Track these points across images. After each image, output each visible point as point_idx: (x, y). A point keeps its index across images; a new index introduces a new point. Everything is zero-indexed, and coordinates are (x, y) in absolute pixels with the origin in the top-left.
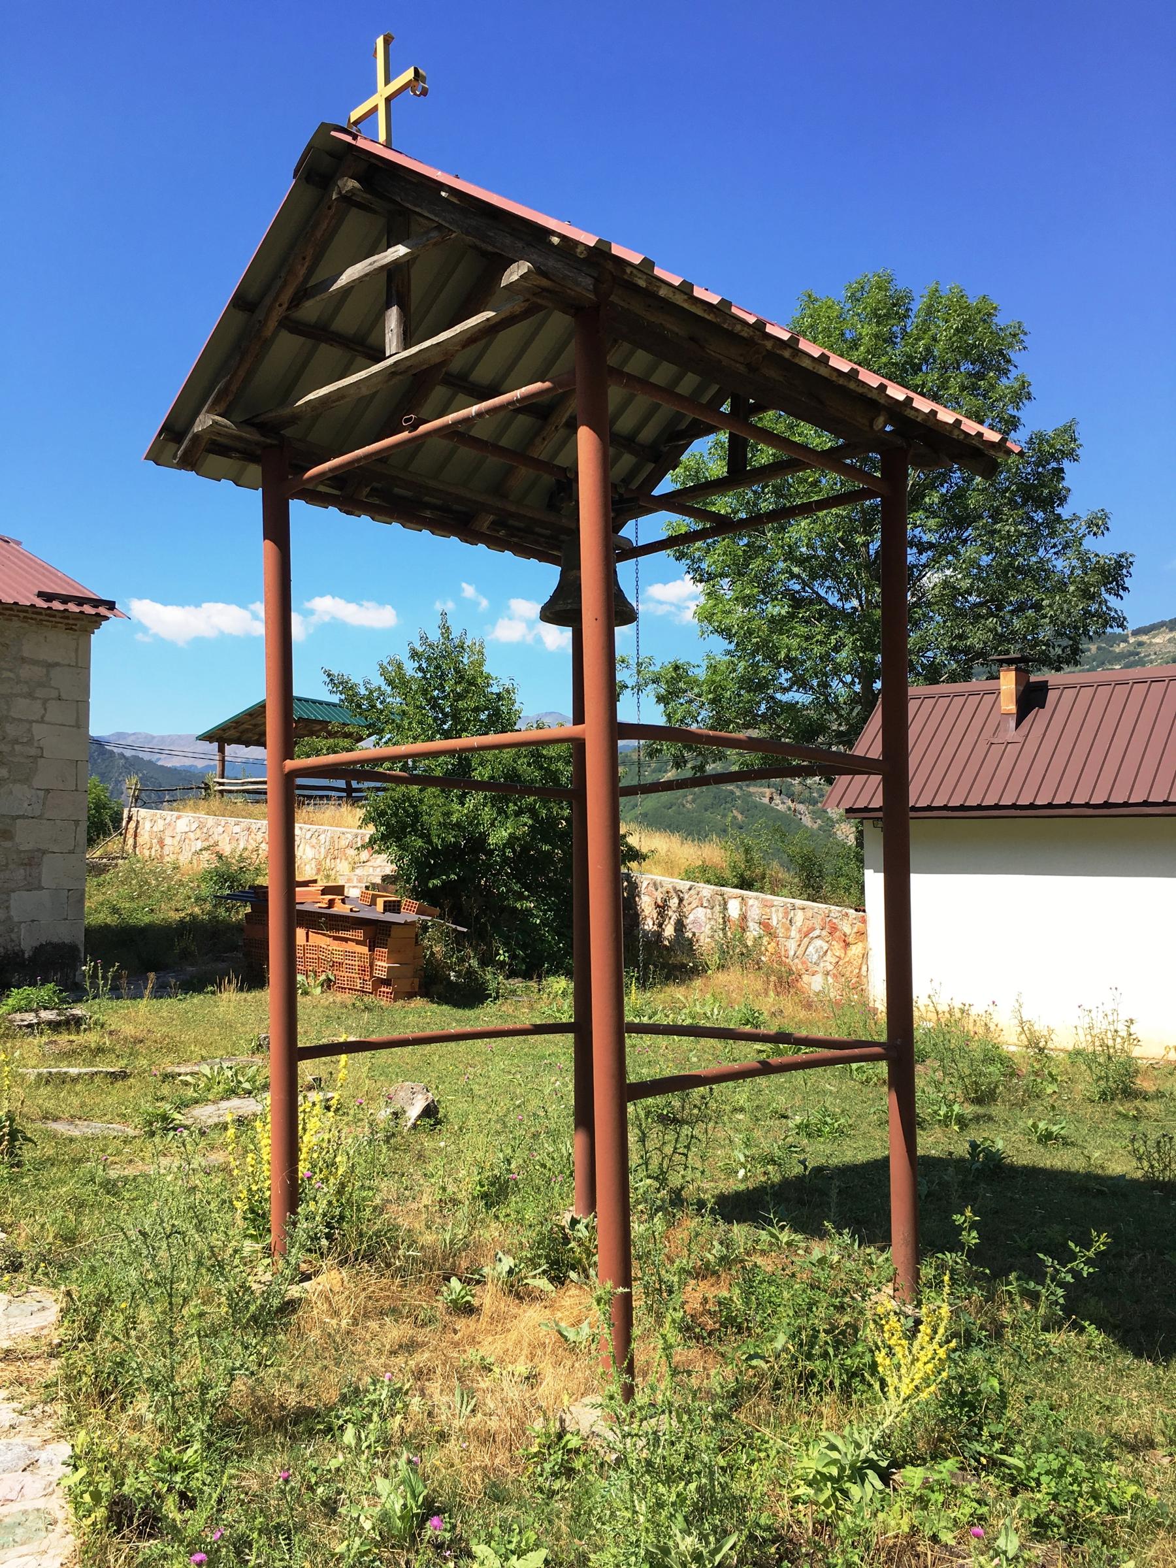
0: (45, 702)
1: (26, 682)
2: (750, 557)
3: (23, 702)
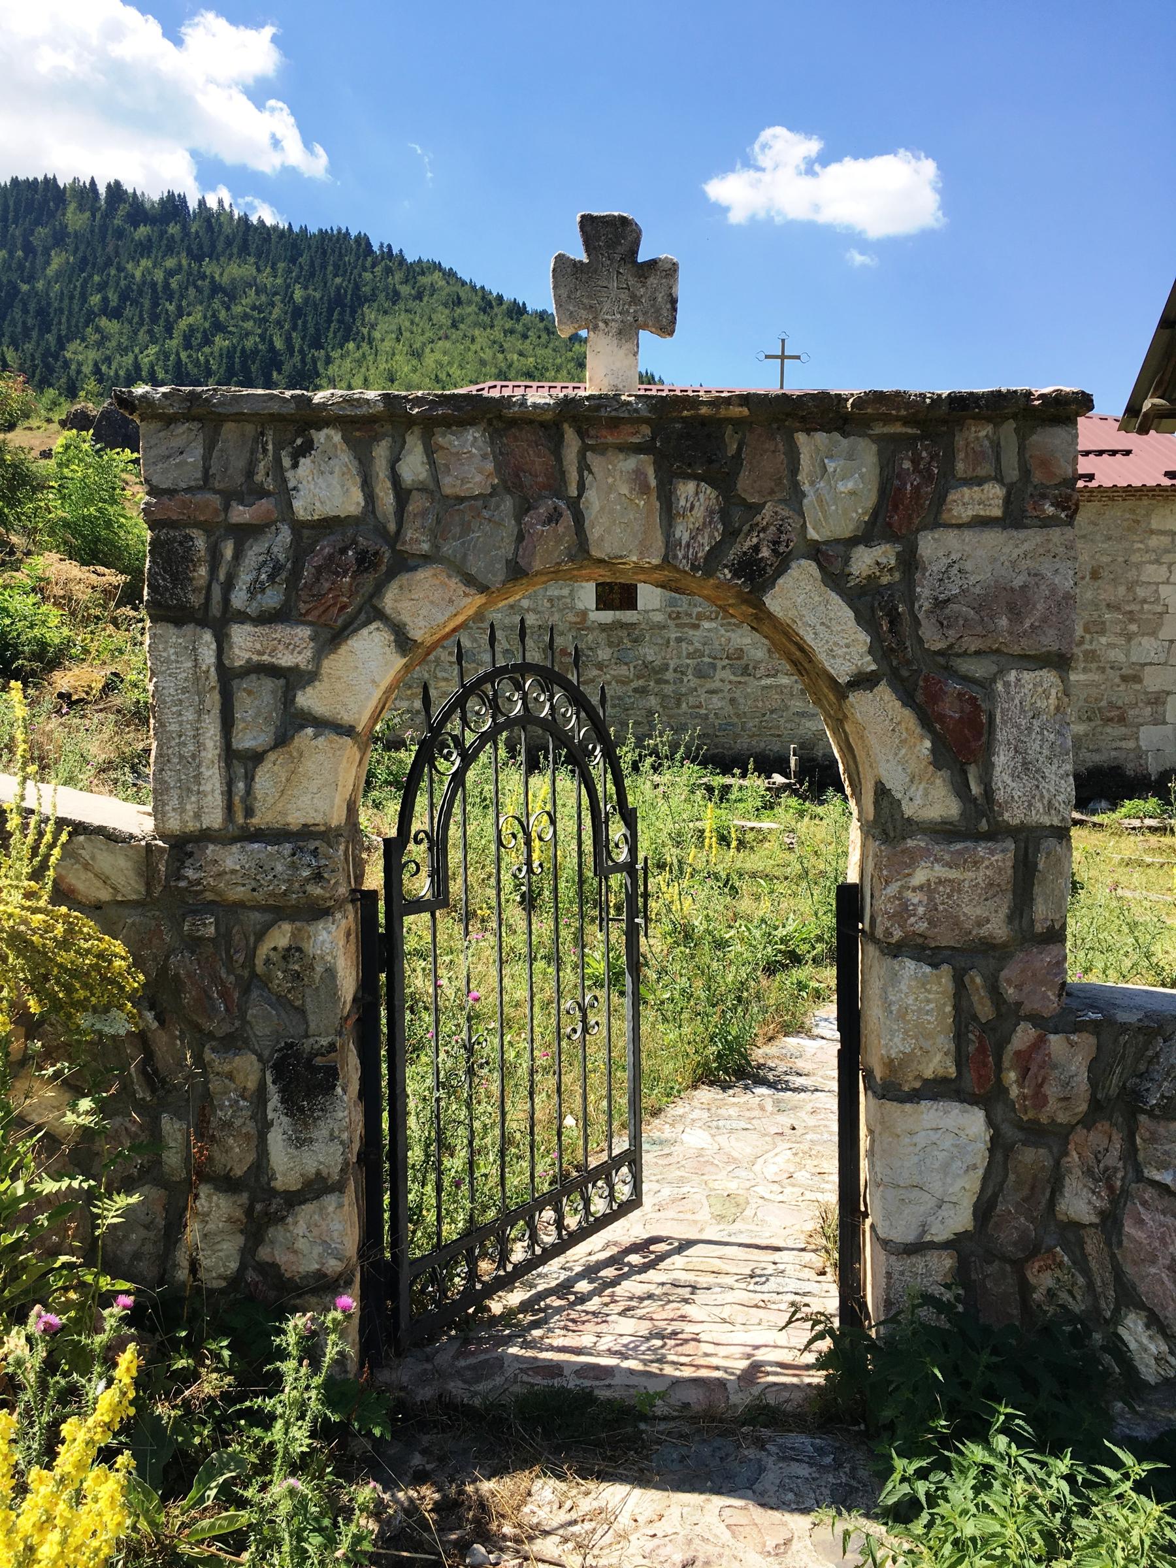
3: (1150, 568)
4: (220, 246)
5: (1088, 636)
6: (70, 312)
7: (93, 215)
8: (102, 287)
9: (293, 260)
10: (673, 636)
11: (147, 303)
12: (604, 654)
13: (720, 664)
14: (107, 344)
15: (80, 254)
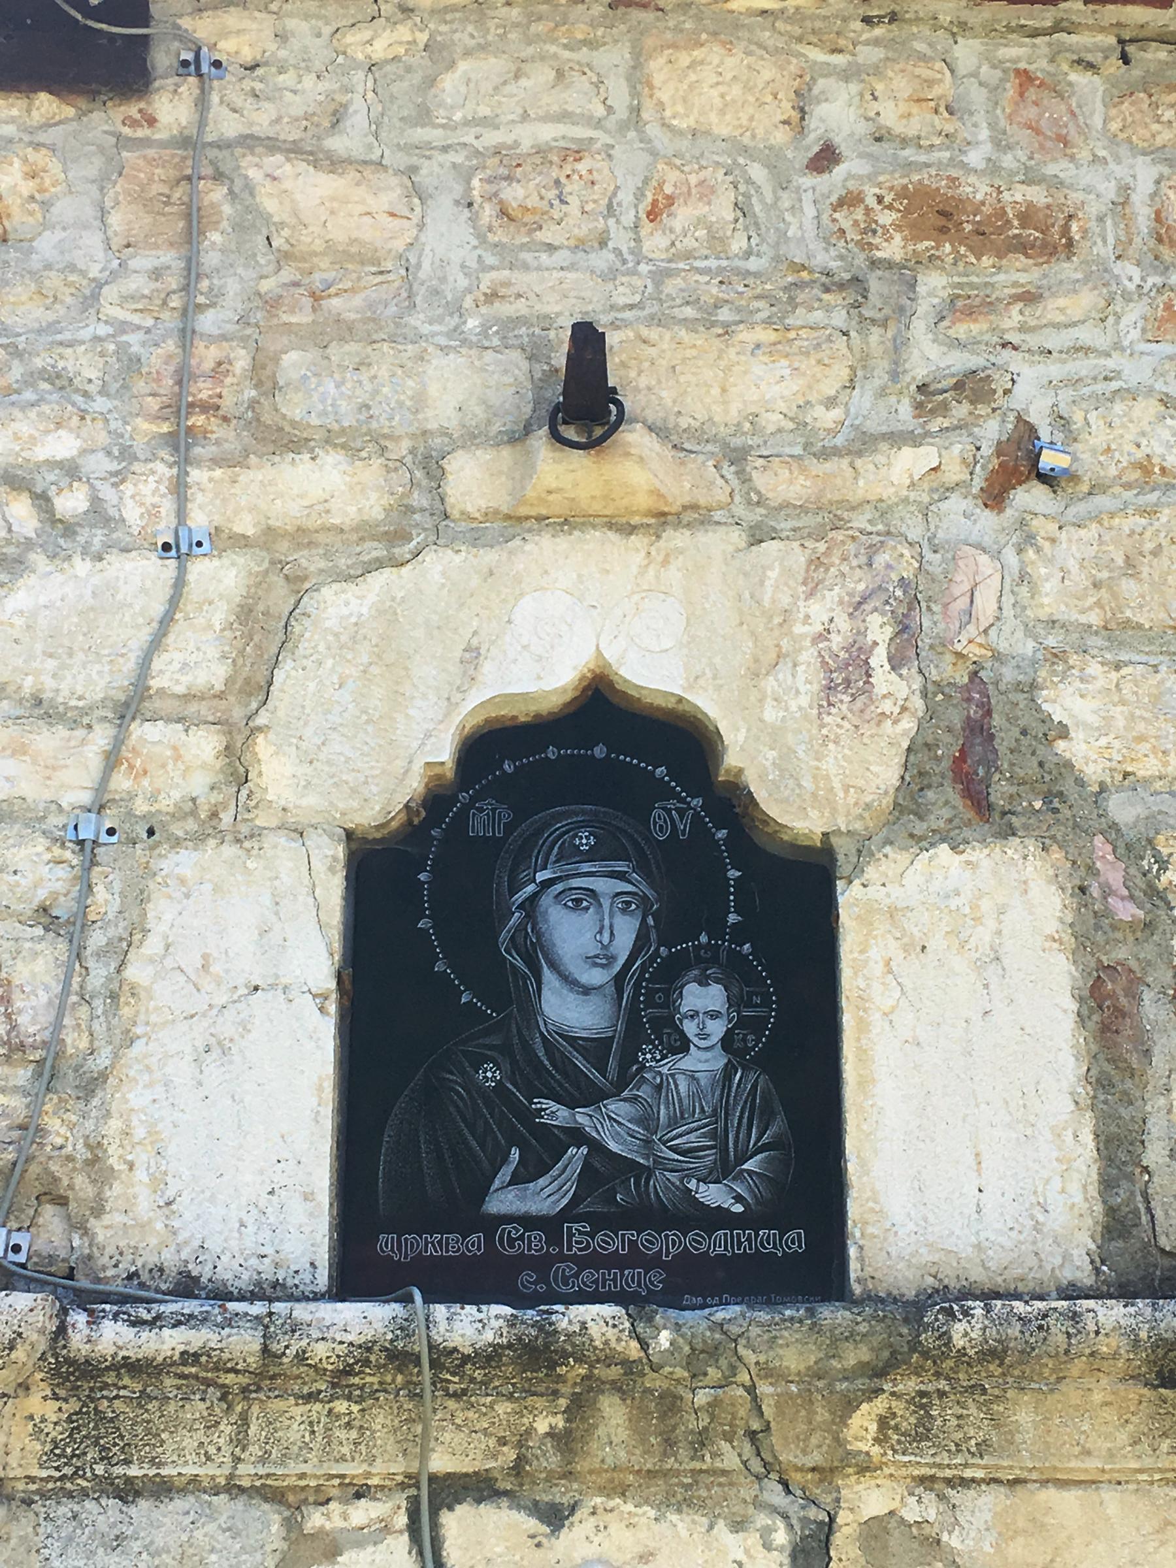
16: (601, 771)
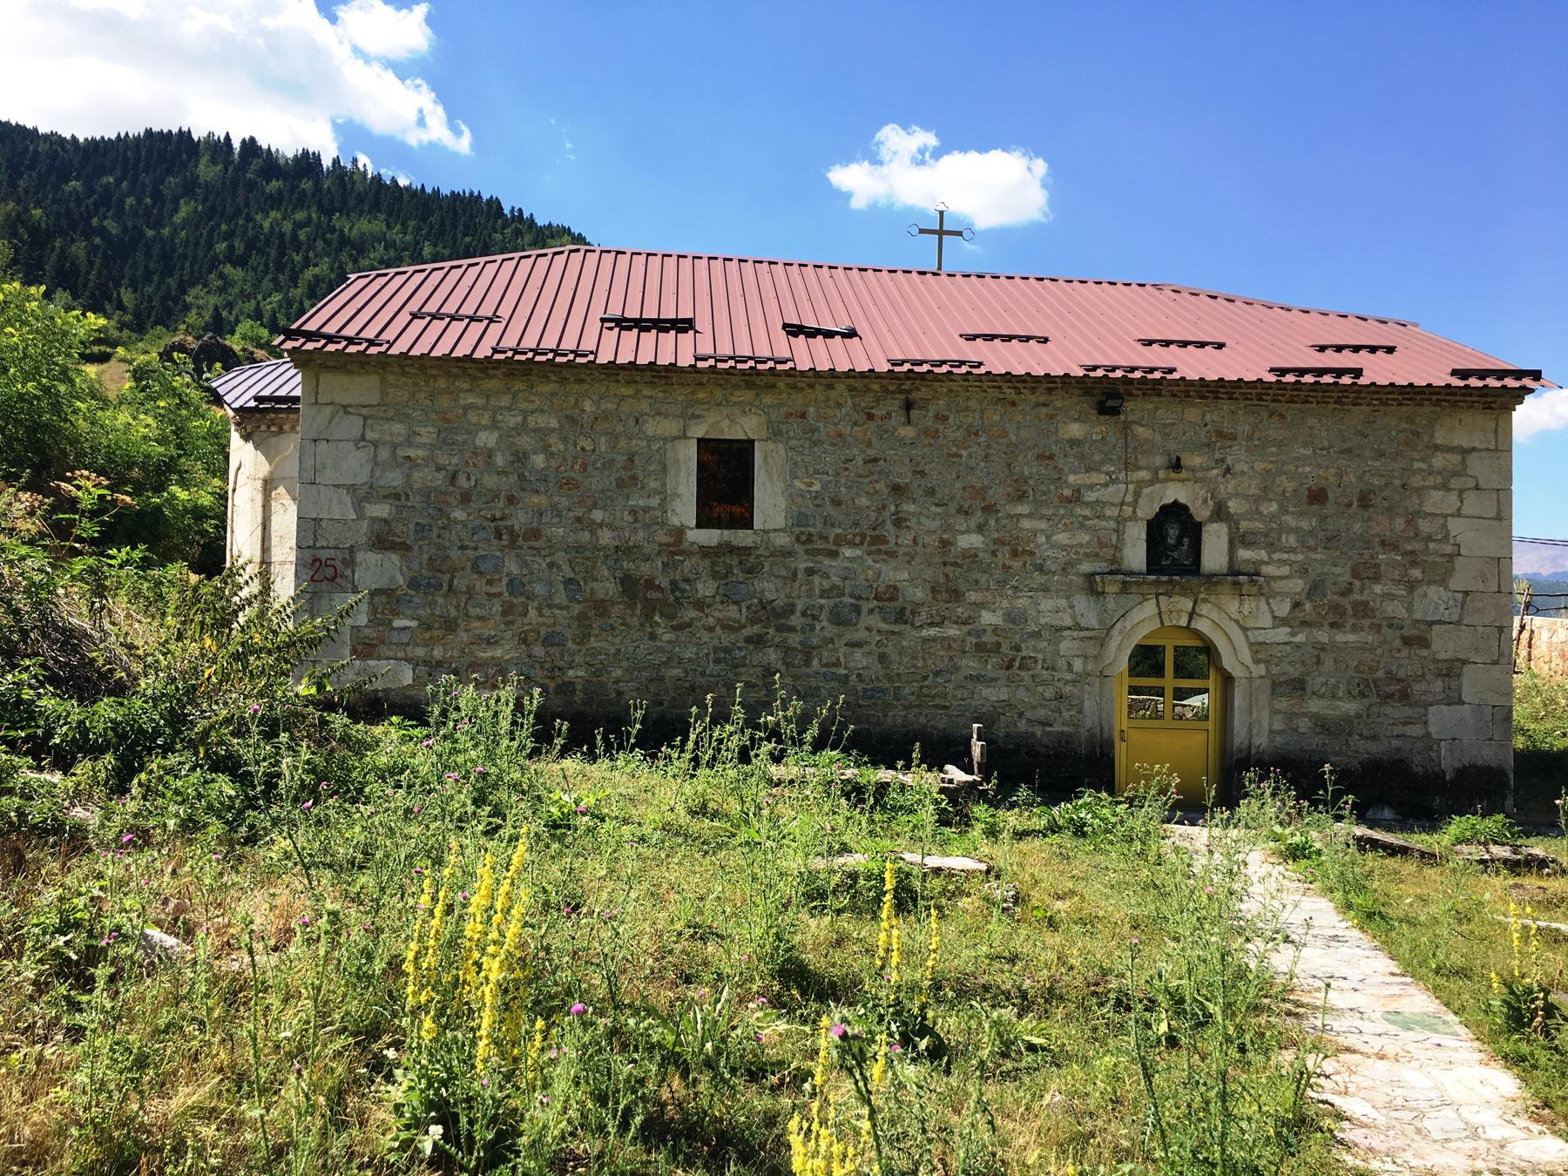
0: (1461, 492)
1: (1439, 473)
2: (226, 765)
3: (1437, 495)
4: (351, 202)
5: (1357, 583)
6: (194, 258)
7: (226, 169)
8: (229, 236)
9: (424, 219)
10: (802, 566)
11: (273, 252)
12: (706, 588)
13: (866, 606)
14: (230, 290)
15: (208, 204)
16: (1174, 512)
